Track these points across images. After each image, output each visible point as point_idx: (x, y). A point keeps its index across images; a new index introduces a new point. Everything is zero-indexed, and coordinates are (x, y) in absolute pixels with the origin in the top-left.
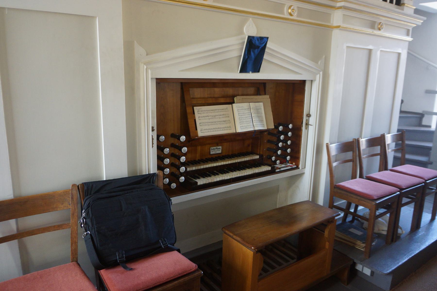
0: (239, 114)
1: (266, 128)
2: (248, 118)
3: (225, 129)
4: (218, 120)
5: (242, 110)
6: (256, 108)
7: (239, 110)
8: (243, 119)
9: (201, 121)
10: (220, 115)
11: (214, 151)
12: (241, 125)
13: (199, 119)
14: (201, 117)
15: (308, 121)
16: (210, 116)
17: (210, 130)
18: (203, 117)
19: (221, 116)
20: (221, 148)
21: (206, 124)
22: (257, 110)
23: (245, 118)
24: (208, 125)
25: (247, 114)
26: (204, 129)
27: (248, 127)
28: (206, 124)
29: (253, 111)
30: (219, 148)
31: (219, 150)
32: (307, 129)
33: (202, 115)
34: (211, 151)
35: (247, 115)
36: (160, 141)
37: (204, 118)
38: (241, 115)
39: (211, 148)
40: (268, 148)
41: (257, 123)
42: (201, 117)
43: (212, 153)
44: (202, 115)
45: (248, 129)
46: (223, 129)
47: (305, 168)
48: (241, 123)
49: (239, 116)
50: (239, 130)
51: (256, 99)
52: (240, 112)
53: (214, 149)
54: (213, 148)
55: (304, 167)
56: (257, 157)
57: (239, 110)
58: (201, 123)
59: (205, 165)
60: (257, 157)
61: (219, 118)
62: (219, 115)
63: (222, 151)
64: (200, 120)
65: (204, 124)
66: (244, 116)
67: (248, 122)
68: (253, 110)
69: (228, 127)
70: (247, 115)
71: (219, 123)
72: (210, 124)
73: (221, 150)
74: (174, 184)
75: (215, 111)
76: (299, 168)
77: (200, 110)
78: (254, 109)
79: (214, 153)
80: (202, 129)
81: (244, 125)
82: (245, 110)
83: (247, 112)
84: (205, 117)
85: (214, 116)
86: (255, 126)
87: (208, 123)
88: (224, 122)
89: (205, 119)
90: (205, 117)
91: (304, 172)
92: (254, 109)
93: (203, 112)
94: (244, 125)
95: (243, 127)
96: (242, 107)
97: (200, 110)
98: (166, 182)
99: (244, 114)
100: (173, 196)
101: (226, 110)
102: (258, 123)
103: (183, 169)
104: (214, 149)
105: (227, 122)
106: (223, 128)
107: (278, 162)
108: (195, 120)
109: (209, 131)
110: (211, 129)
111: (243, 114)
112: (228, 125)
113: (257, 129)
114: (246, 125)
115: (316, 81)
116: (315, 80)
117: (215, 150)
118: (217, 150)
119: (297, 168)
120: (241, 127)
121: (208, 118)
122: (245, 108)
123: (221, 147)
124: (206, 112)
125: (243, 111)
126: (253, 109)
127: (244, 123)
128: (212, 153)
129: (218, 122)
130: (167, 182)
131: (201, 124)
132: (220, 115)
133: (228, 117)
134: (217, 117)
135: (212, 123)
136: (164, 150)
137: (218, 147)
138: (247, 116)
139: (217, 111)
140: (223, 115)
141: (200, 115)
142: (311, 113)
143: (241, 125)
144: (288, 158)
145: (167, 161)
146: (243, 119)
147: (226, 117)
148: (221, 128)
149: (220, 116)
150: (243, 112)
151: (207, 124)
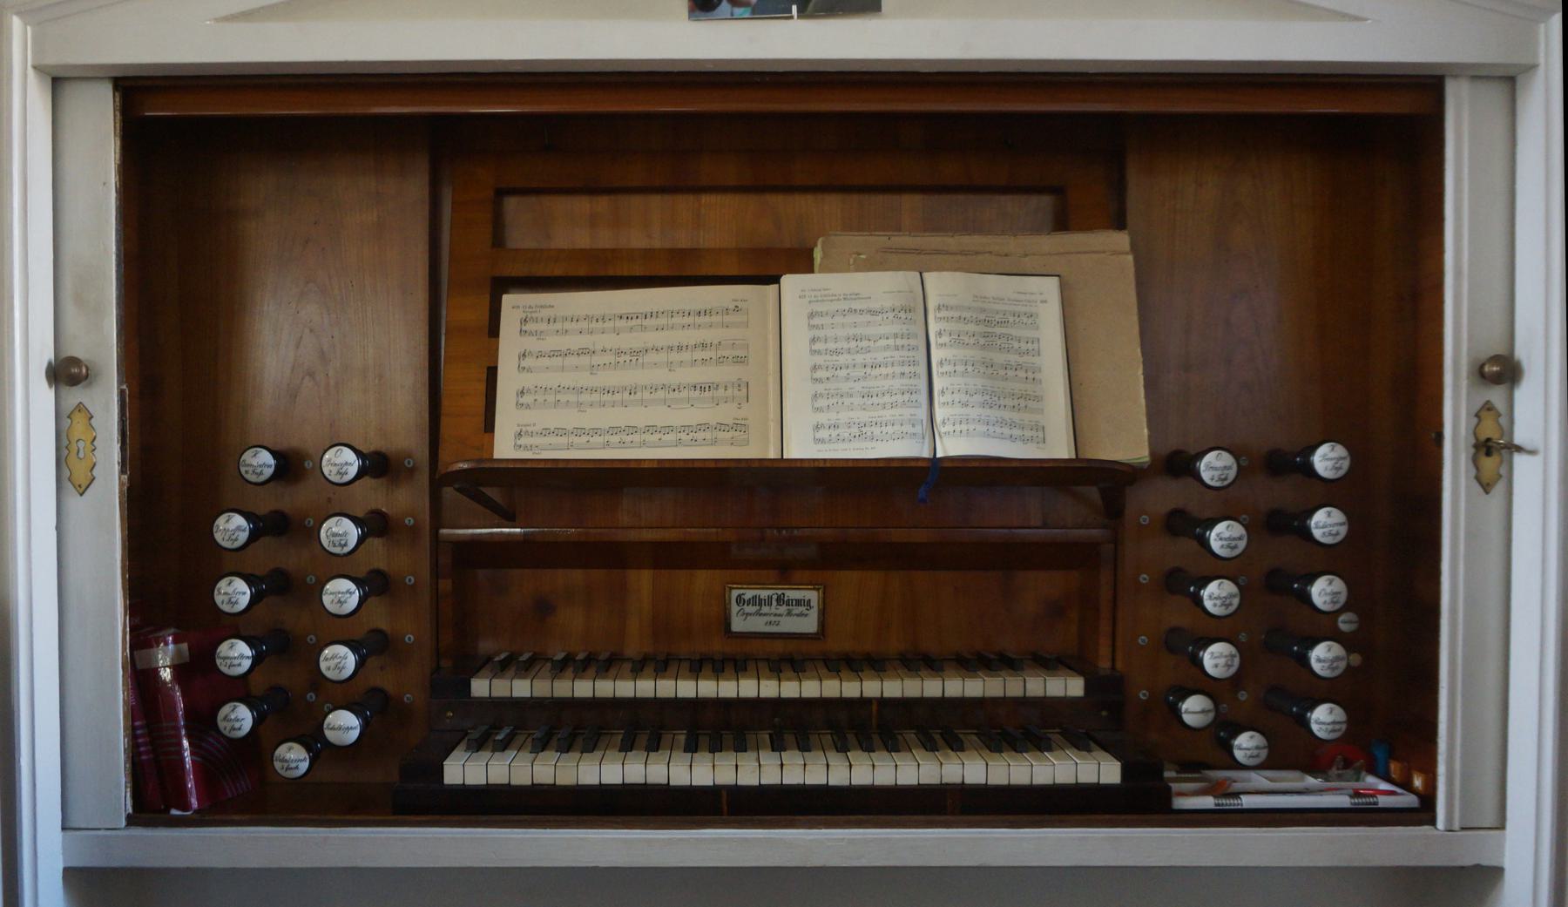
0: (813, 340)
1: (1059, 448)
2: (890, 370)
3: (700, 436)
4: (661, 376)
5: (851, 319)
6: (983, 310)
7: (821, 314)
8: (843, 373)
9: (528, 380)
10: (680, 348)
11: (759, 614)
12: (822, 418)
13: (521, 369)
14: (540, 355)
15: (1503, 421)
16: (604, 351)
17: (584, 439)
18: (554, 354)
19: (686, 356)
20: (814, 603)
21: (559, 397)
22: (987, 322)
23: (859, 372)
24: (579, 404)
25: (883, 342)
26: (538, 428)
27: (877, 431)
28: (563, 398)
29: (943, 325)
30: (799, 602)
31: (801, 615)
32: (1499, 489)
33: (553, 342)
34: (735, 608)
35: (887, 347)
36: (246, 476)
37: (557, 361)
38: (832, 346)
39: (735, 593)
40: (1174, 630)
41: (968, 410)
42: (540, 355)
43: (738, 625)
44: (553, 342)
45: (874, 444)
46: (683, 436)
47: (1502, 826)
48: (822, 403)
49: (814, 352)
50: (801, 446)
51: (1006, 255)
52: (833, 326)
53: (756, 601)
54: (749, 594)
55: (1489, 819)
56: (1074, 687)
57: (821, 314)
58: (529, 390)
59: (605, 678)
60: (1074, 687)
61: (670, 364)
62: (671, 348)
63: (822, 624)
64: (530, 370)
65: (551, 398)
66: (859, 358)
67: (887, 399)
68: (947, 319)
69: (721, 427)
70: (887, 347)
71: (661, 394)
72: (596, 397)
73: (814, 615)
74: (290, 749)
75: (647, 322)
76: (1432, 821)
77: (545, 313)
78: (956, 314)
79: (758, 630)
80: (530, 429)
81: (844, 417)
82: (868, 317)
83: (883, 330)
84: (568, 353)
85: (636, 353)
86: (941, 428)
87: (580, 390)
88: (702, 389)
89: (563, 369)
90: (568, 353)
91: (1486, 861)
92: (956, 314)
93: (558, 326)
94: (844, 417)
95: (834, 433)
96: (857, 296)
97: (545, 313)
98: (229, 725)
99: (864, 344)
100: (236, 817)
101: (727, 319)
102: (974, 413)
103: (333, 658)
104: (756, 601)
105: (721, 391)
106: (684, 428)
107: (1246, 744)
108: (492, 373)
109: (577, 440)
110: (596, 431)
111: (853, 344)
112: (726, 413)
113: (952, 446)
114: (864, 416)
115: (1541, 71)
116: (1531, 68)
117: (765, 609)
118: (783, 609)
119: (1424, 811)
120: (817, 427)
121: (585, 360)
122: (875, 306)
123: (812, 596)
124: (583, 325)
125: (855, 325)
126: (943, 314)
127: (847, 401)
128: (738, 625)
129: (654, 389)
130: (237, 725)
131: (526, 399)
132: (680, 348)
133: (740, 360)
134: (651, 357)
135: (607, 397)
136: (214, 522)
137: (792, 594)
138: (880, 356)
139: (662, 321)
140: (704, 346)
141: (531, 344)
142: (1520, 353)
143: (822, 418)
144: (1324, 718)
145: (230, 590)
146: (847, 379)
147: (721, 360)
148: (669, 429)
149: (675, 357)
150: (852, 331)
151: (572, 398)
